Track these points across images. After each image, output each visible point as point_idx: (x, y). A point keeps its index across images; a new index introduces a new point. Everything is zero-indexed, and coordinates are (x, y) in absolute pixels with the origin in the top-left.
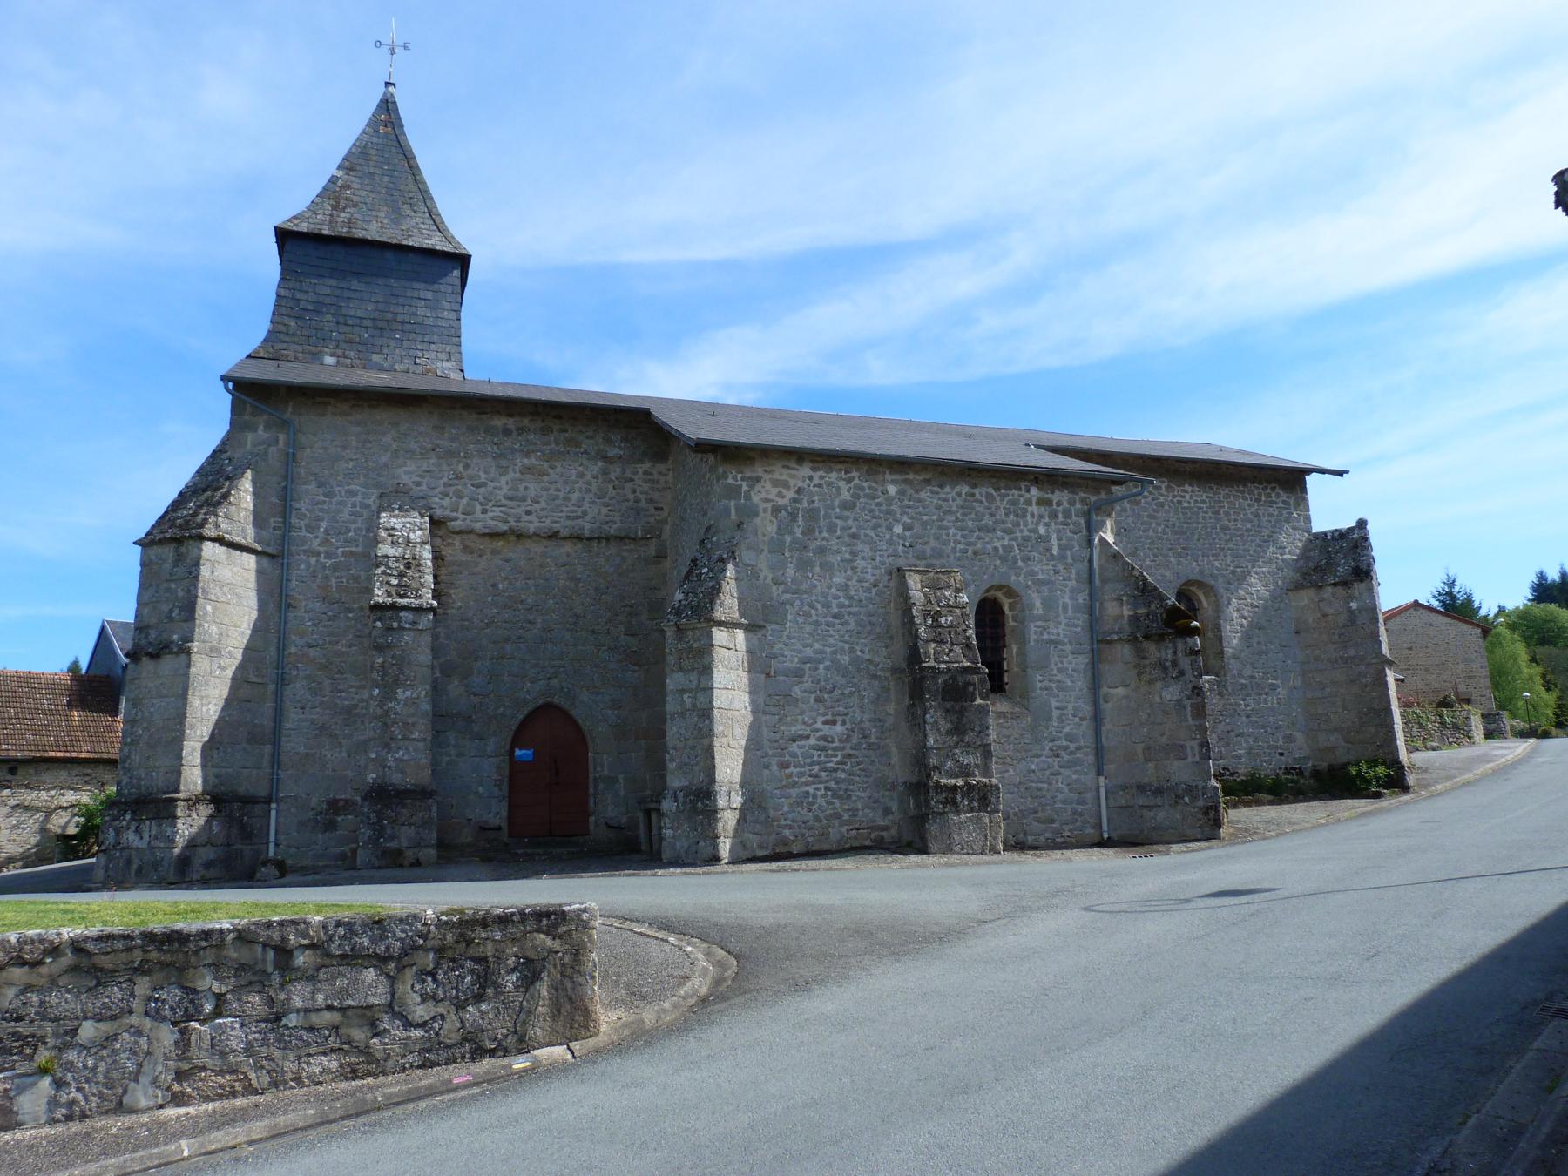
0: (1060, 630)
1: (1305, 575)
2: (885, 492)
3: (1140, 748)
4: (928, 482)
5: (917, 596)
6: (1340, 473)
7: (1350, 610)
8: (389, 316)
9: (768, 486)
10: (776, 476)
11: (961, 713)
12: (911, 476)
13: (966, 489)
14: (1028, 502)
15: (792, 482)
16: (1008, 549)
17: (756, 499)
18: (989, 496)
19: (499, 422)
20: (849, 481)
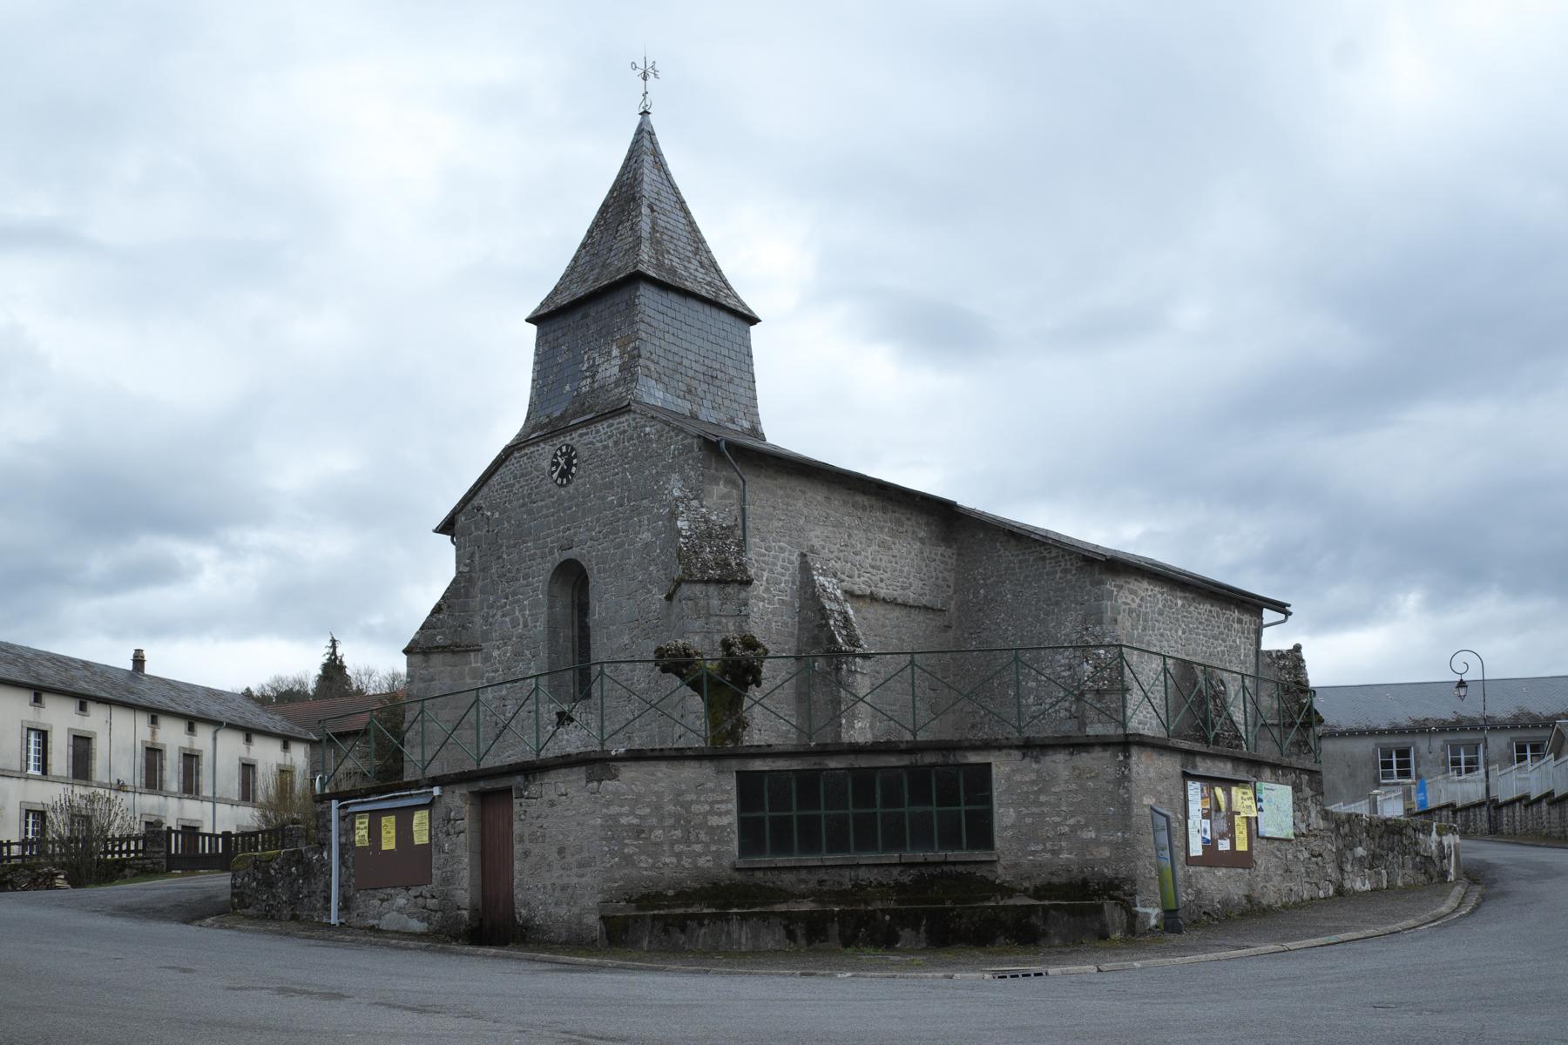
19: (860, 499)
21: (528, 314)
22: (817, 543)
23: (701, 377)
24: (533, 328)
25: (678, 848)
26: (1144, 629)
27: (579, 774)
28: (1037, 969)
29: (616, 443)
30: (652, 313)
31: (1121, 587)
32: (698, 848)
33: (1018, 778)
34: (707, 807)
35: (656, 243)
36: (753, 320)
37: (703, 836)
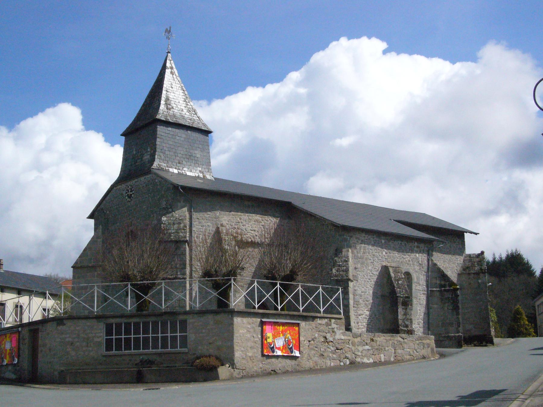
0: (420, 288)
1: (464, 270)
2: (381, 242)
3: (440, 323)
4: (391, 239)
5: (392, 275)
6: (476, 234)
7: (479, 283)
8: (190, 154)
9: (354, 239)
10: (357, 236)
11: (406, 309)
12: (387, 238)
13: (400, 242)
14: (414, 247)
15: (360, 238)
16: (409, 261)
17: (351, 242)
18: (405, 244)
19: (246, 203)
20: (373, 238)
21: (122, 132)
22: (224, 223)
23: (184, 156)
24: (124, 138)
25: (84, 349)
26: (364, 253)
27: (95, 320)
28: (157, 387)
29: (146, 186)
30: (163, 134)
31: (351, 237)
32: (90, 349)
33: (196, 324)
34: (94, 335)
35: (167, 104)
36: (211, 132)
37: (92, 345)
